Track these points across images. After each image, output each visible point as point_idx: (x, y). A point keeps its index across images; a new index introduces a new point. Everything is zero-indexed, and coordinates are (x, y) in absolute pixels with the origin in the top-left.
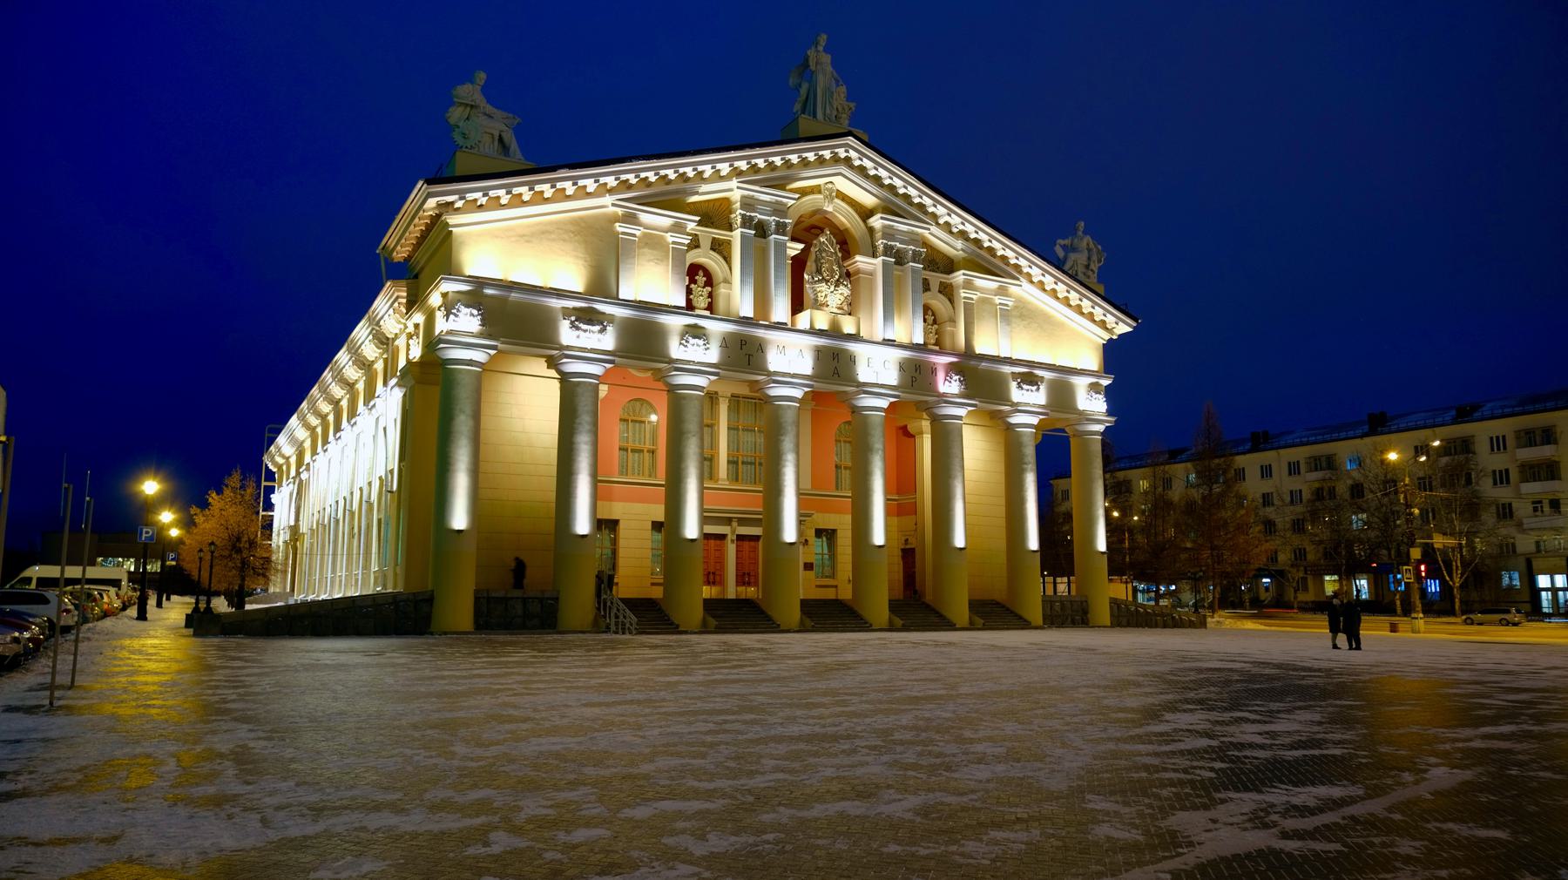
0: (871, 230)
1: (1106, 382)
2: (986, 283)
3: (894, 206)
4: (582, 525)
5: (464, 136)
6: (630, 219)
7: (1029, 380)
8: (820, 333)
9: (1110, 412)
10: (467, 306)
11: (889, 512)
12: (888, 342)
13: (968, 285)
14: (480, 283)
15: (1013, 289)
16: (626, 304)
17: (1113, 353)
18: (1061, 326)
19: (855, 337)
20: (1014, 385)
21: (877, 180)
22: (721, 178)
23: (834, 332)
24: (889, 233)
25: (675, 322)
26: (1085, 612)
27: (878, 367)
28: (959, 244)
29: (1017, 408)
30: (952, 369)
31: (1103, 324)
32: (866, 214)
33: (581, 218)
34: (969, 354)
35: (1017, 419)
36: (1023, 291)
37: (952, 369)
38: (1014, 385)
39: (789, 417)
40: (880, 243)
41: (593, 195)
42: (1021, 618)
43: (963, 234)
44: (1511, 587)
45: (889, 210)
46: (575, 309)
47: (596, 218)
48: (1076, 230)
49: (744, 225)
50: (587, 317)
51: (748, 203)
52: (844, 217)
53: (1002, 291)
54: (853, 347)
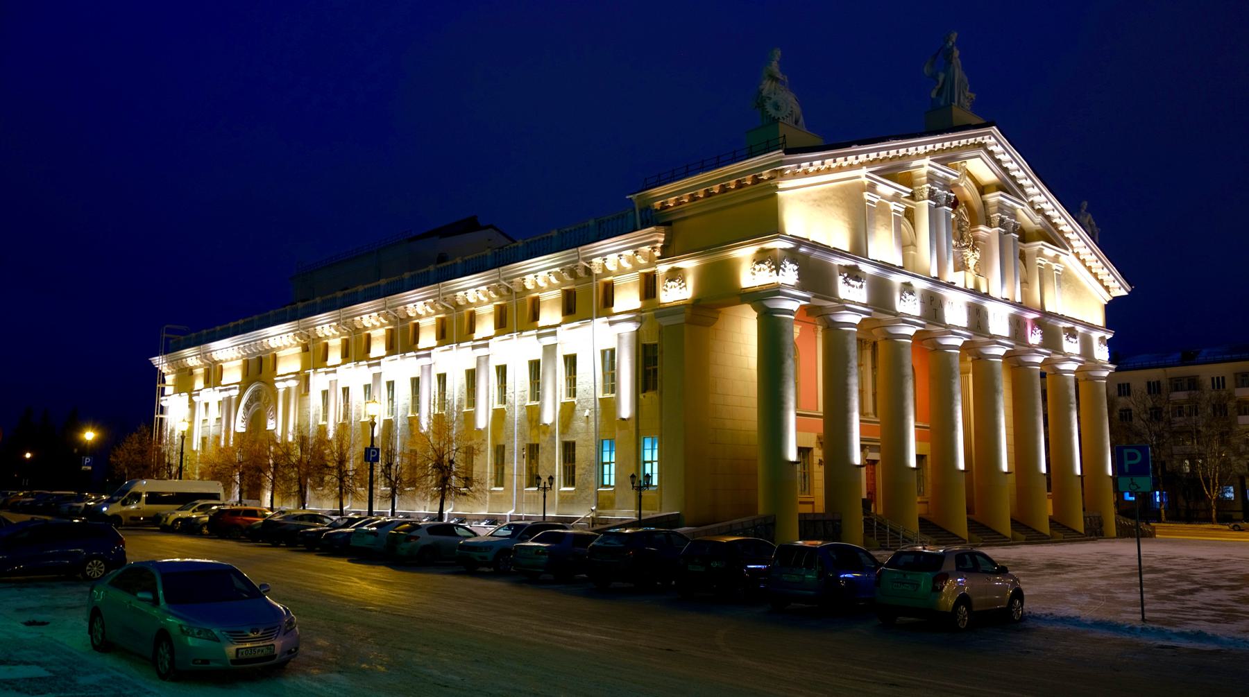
0: (985, 203)
1: (1109, 336)
2: (1049, 251)
3: (1007, 185)
4: (792, 455)
5: (777, 107)
6: (872, 188)
7: (1072, 333)
8: (1014, 304)
9: (1111, 361)
10: (791, 262)
11: (798, 429)
12: (1006, 301)
13: (1040, 253)
14: (800, 241)
15: (1063, 258)
16: (875, 263)
17: (1114, 309)
18: (1083, 289)
19: (951, 286)
20: (840, 279)
21: (998, 162)
22: (921, 157)
23: (975, 291)
24: (1001, 207)
25: (897, 279)
26: (1101, 524)
27: (999, 321)
28: (1039, 219)
29: (843, 305)
30: (1037, 323)
31: (1107, 288)
32: (983, 189)
33: (845, 186)
34: (1042, 311)
35: (1063, 367)
36: (1068, 260)
37: (1037, 323)
38: (840, 279)
39: (957, 363)
40: (996, 216)
41: (854, 168)
42: (949, 533)
43: (1040, 211)
44: (273, 432)
45: (1001, 187)
46: (846, 267)
47: (852, 185)
48: (1080, 208)
49: (930, 198)
50: (853, 274)
51: (931, 178)
52: (968, 191)
53: (1056, 259)
54: (945, 292)
